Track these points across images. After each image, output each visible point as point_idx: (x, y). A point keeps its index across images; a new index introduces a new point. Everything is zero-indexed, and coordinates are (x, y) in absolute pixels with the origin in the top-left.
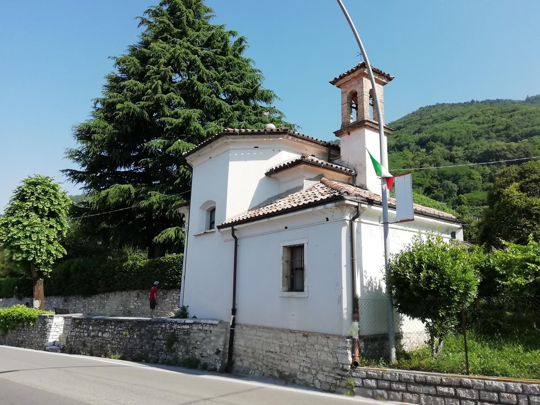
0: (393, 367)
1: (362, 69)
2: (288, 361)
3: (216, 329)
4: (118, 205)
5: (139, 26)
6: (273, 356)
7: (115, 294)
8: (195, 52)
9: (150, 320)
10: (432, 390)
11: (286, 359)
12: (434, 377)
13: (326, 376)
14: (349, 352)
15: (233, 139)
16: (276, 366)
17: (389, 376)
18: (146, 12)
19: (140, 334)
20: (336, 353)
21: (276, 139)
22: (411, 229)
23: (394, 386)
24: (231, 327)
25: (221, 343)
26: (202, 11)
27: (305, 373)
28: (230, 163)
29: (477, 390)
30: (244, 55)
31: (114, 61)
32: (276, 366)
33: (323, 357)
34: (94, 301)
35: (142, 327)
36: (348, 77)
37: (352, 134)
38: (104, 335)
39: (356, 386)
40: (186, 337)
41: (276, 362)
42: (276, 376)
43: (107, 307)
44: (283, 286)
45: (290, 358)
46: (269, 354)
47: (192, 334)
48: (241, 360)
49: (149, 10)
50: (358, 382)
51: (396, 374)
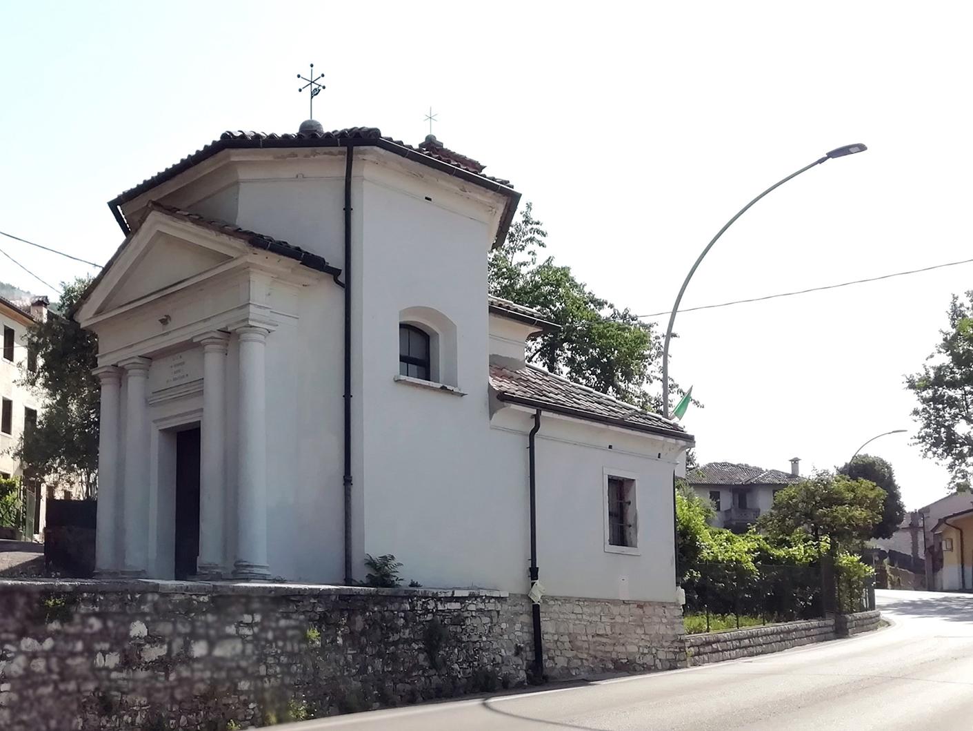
2: (623, 645)
3: (505, 607)
6: (604, 640)
11: (622, 641)
13: (666, 652)
16: (609, 655)
20: (674, 623)
25: (520, 633)
27: (645, 654)
32: (609, 655)
33: (662, 630)
35: (352, 612)
38: (218, 652)
41: (608, 648)
42: (610, 668)
45: (626, 639)
47: (468, 622)
48: (552, 658)
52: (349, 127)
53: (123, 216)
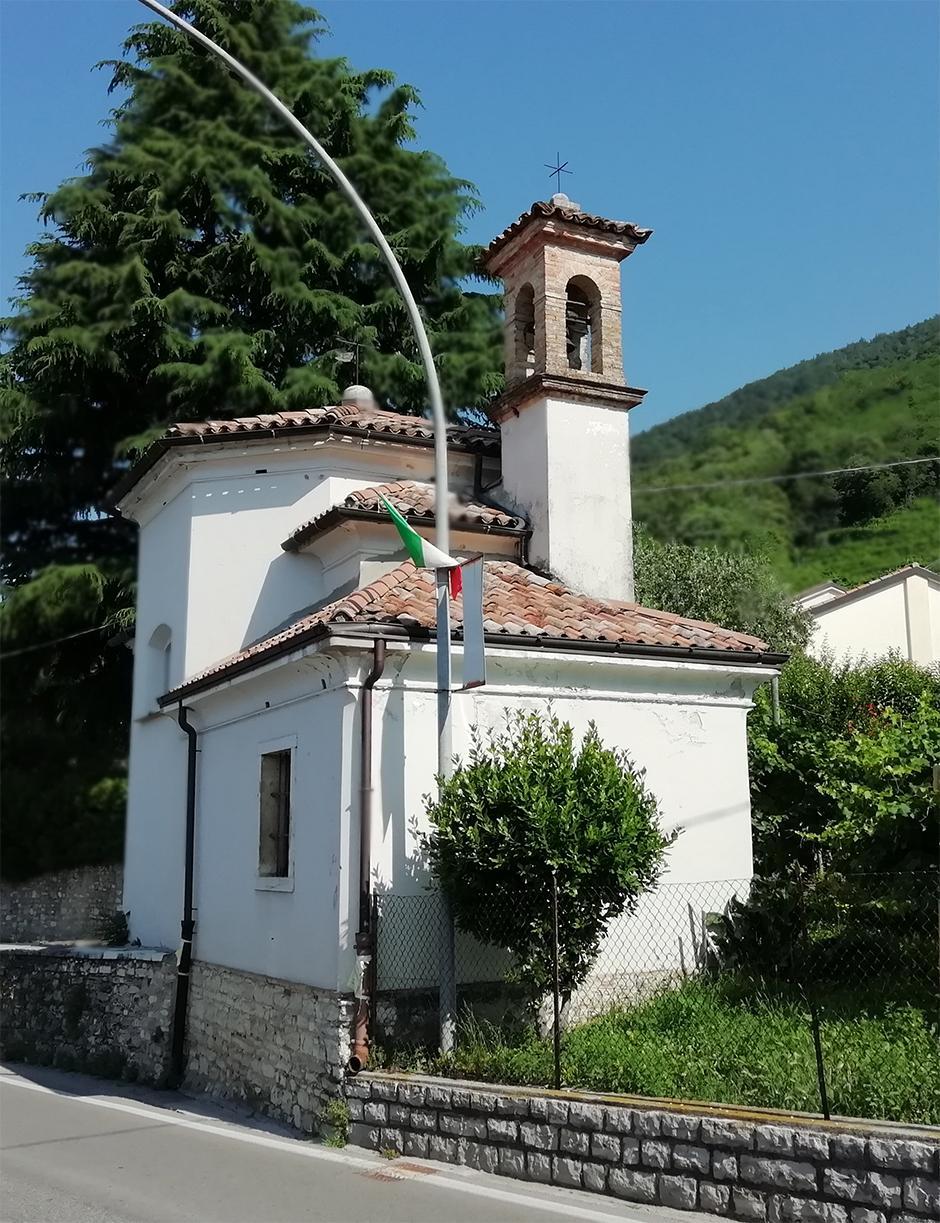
0: (447, 1071)
1: (537, 223)
3: (160, 975)
4: (69, 621)
5: (111, 89)
7: (81, 874)
8: (251, 158)
9: (40, 952)
10: (479, 1128)
12: (485, 1095)
14: (343, 1033)
15: (196, 453)
17: (408, 1092)
18: (128, 45)
19: (22, 988)
21: (307, 446)
22: (591, 693)
23: (416, 1118)
24: (181, 968)
26: (281, 21)
28: (195, 520)
29: (555, 1125)
30: (407, 146)
31: (39, 206)
34: (34, 895)
36: (511, 245)
37: (523, 412)
39: (351, 1121)
40: (105, 997)
43: (64, 910)
44: (262, 861)
46: (236, 1040)
49: (135, 37)
50: (355, 1111)
51: (420, 1088)
52: (810, 356)
53: (878, 580)
